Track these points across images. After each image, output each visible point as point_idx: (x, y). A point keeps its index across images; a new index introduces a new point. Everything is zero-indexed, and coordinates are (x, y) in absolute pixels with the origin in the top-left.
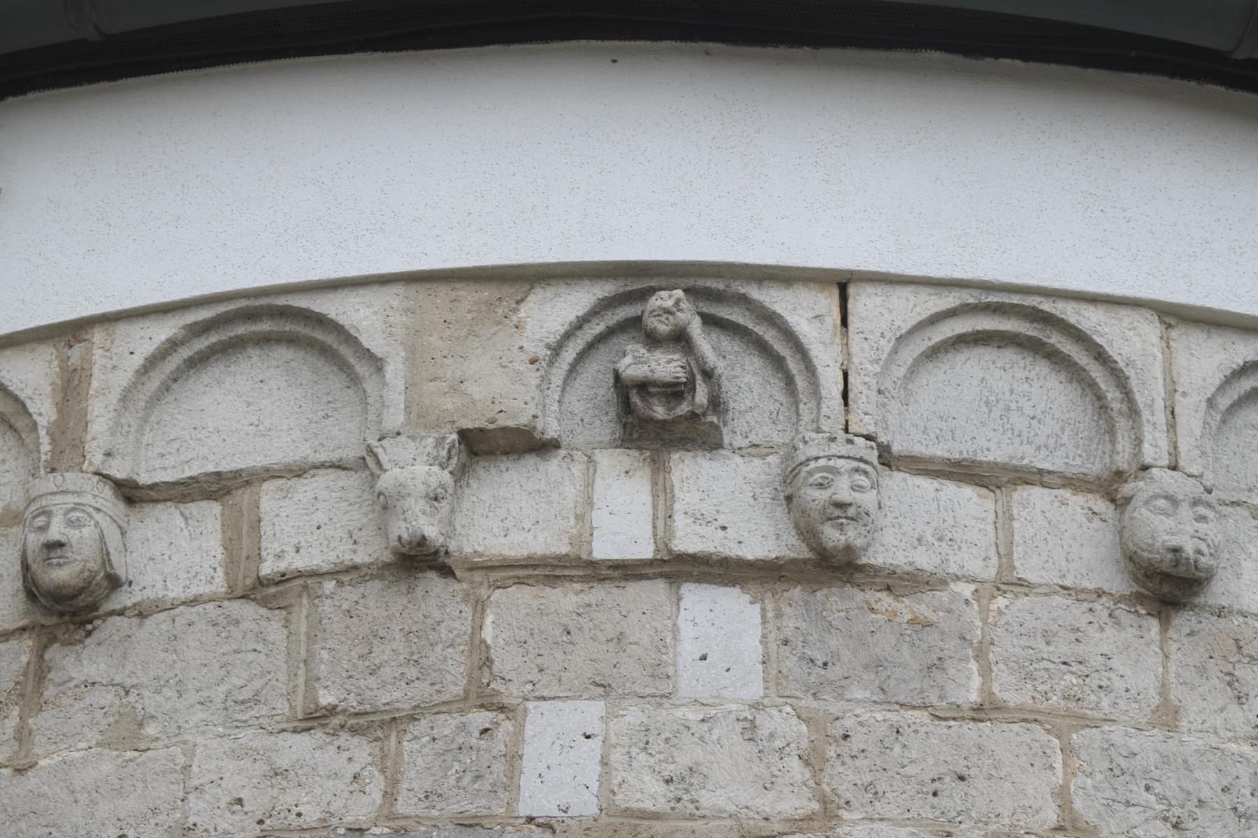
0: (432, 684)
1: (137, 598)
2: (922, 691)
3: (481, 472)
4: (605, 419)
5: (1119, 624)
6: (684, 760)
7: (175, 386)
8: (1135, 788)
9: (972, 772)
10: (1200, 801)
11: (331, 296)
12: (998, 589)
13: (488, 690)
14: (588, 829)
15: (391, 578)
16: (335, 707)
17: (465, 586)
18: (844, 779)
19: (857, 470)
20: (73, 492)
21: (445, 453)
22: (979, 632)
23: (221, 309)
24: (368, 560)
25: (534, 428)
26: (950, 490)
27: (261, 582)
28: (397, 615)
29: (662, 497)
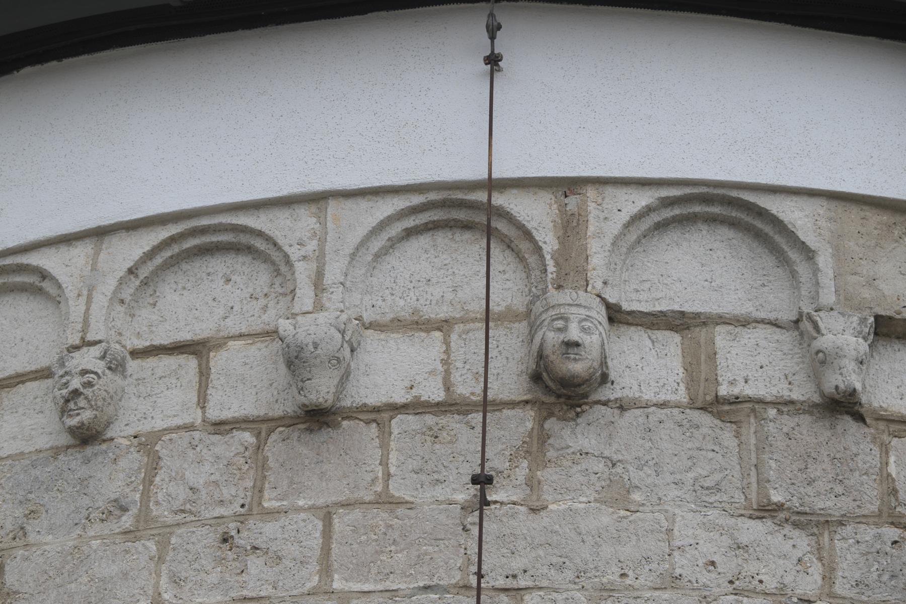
0: (854, 500)
1: (618, 394)
3: (881, 348)
7: (643, 241)
15: (818, 415)
16: (783, 505)
20: (585, 307)
23: (688, 191)
24: (802, 398)
27: (718, 400)
28: (824, 443)
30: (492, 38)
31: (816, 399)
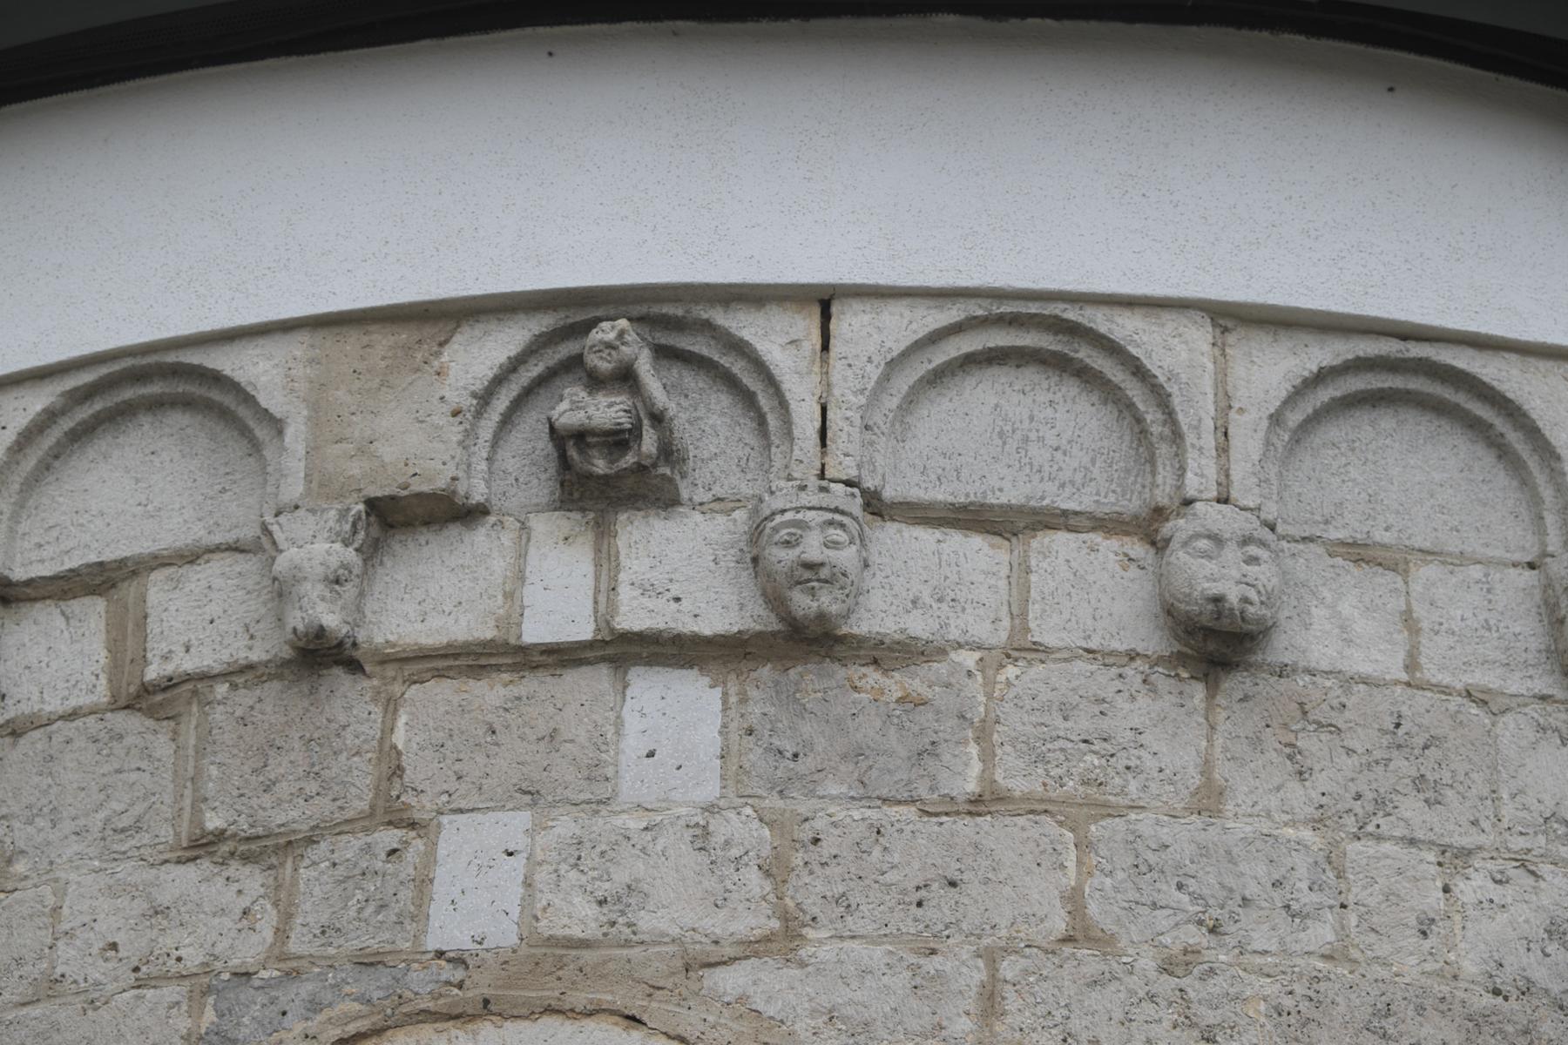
2: (910, 782)
3: (397, 547)
4: (543, 477)
5: (1155, 692)
6: (621, 877)
7: (57, 464)
8: (1164, 887)
9: (965, 877)
10: (1244, 899)
11: (227, 348)
12: (1008, 656)
13: (397, 804)
14: (506, 962)
16: (223, 831)
17: (375, 682)
18: (809, 891)
19: (831, 523)
21: (348, 527)
22: (982, 709)
23: (104, 370)
24: (265, 657)
25: (454, 492)
26: (956, 541)
27: (147, 690)
29: (605, 566)
31: (287, 653)
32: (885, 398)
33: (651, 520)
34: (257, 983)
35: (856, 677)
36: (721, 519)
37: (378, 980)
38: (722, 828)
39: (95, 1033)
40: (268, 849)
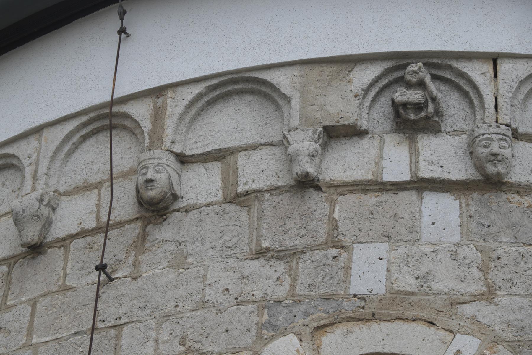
0: (312, 237)
1: (185, 204)
3: (334, 145)
4: (388, 121)
6: (424, 269)
7: (202, 113)
11: (268, 71)
14: (381, 300)
15: (294, 192)
16: (269, 248)
17: (326, 194)
18: (498, 277)
19: (501, 139)
20: (158, 158)
21: (317, 136)
23: (221, 79)
24: (284, 184)
25: (356, 125)
27: (238, 195)
28: (297, 208)
29: (414, 154)
30: (122, 19)
31: (292, 183)
32: (518, 95)
33: (431, 137)
34: (284, 305)
35: (510, 198)
36: (457, 138)
37: (331, 305)
38: (464, 252)
39: (222, 322)
40: (286, 255)
